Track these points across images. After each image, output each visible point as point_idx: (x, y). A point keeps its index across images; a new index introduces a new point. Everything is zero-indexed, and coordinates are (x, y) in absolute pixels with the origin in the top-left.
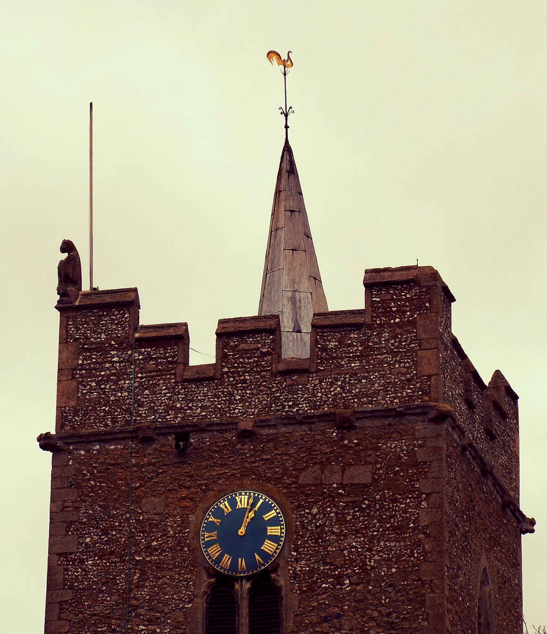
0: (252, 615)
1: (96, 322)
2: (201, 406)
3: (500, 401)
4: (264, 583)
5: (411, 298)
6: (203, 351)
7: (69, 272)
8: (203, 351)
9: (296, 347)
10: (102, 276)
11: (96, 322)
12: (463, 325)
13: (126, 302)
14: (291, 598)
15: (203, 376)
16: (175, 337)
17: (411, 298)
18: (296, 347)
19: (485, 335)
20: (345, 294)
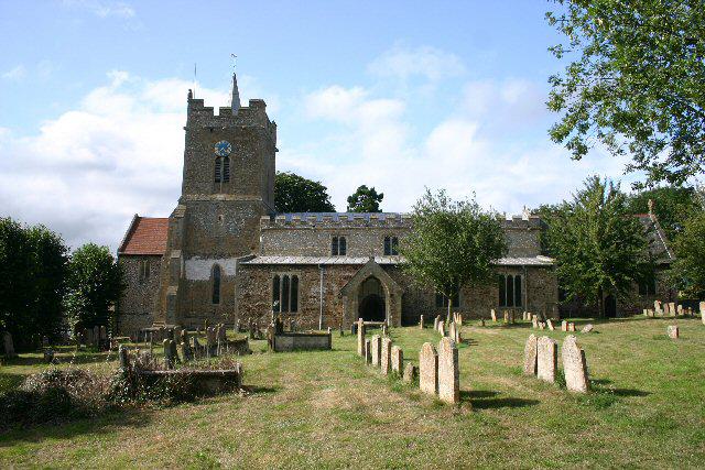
0: (27, 352)
1: (195, 105)
2: (213, 124)
3: (274, 126)
4: (510, 304)
5: (258, 105)
6: (216, 113)
7: (190, 95)
8: (216, 113)
9: (235, 113)
10: (196, 96)
11: (195, 105)
12: (267, 110)
13: (201, 102)
14: (330, 248)
15: (217, 118)
16: (211, 109)
17: (258, 105)
18: (235, 113)
19: (271, 112)
20: (245, 103)
